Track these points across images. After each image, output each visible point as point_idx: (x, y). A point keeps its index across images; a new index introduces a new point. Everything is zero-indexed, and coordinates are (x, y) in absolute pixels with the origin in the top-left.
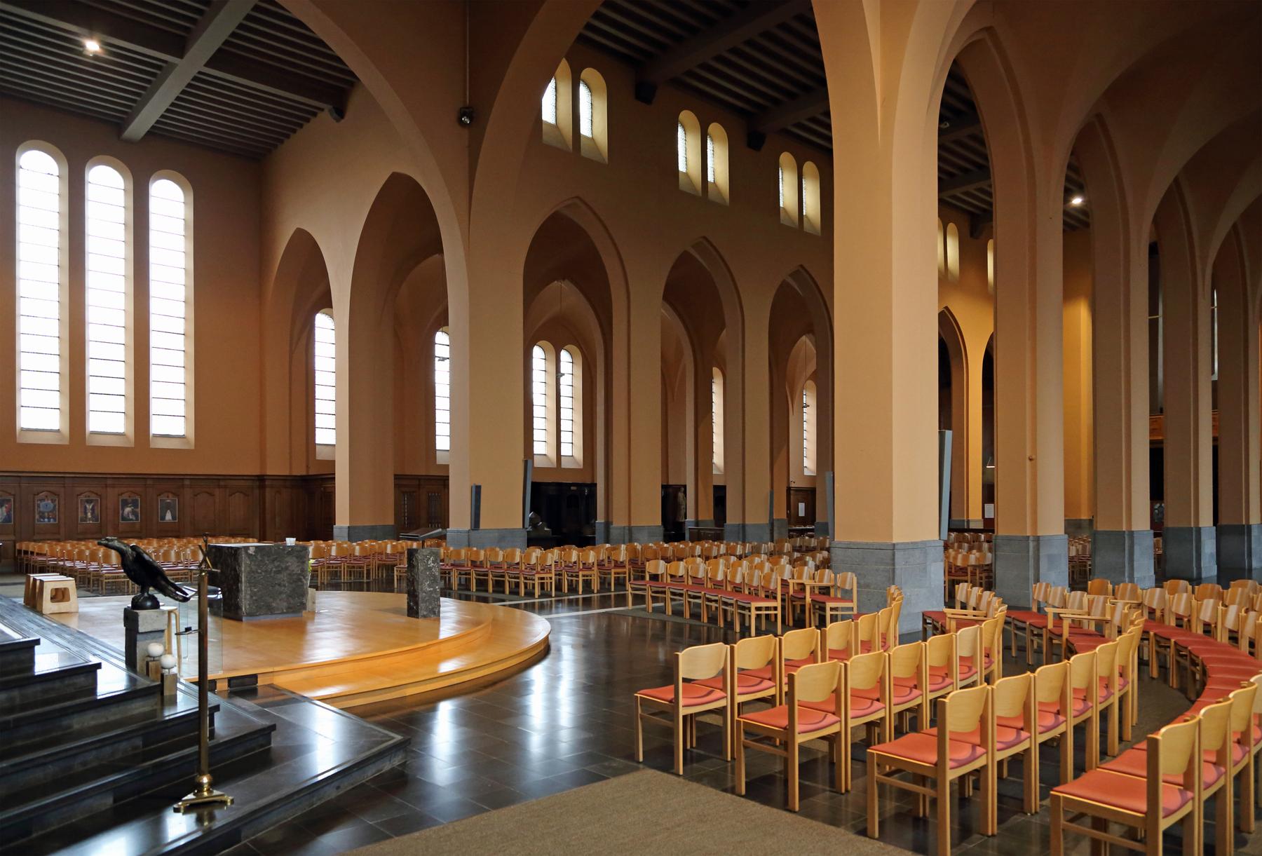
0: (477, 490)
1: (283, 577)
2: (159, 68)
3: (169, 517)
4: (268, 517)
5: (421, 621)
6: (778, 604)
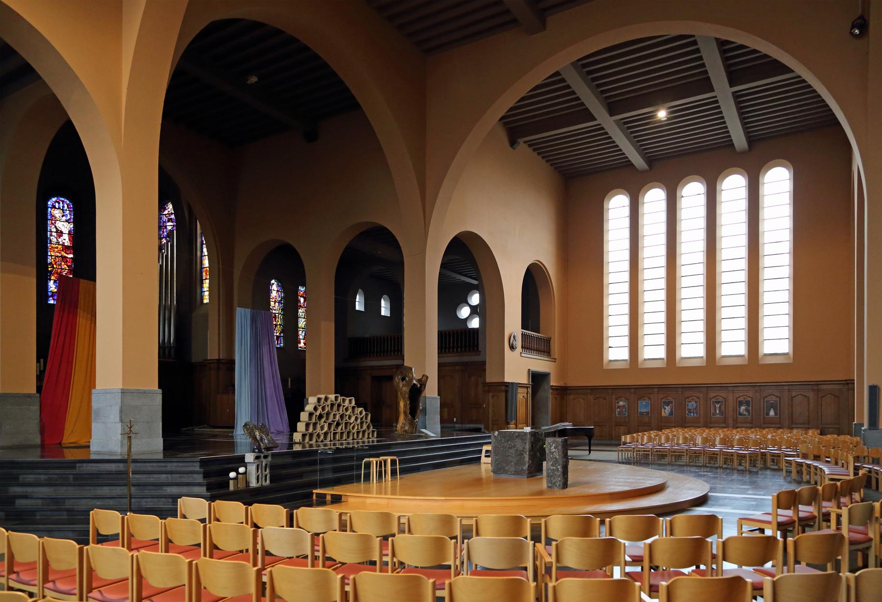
3: (772, 413)
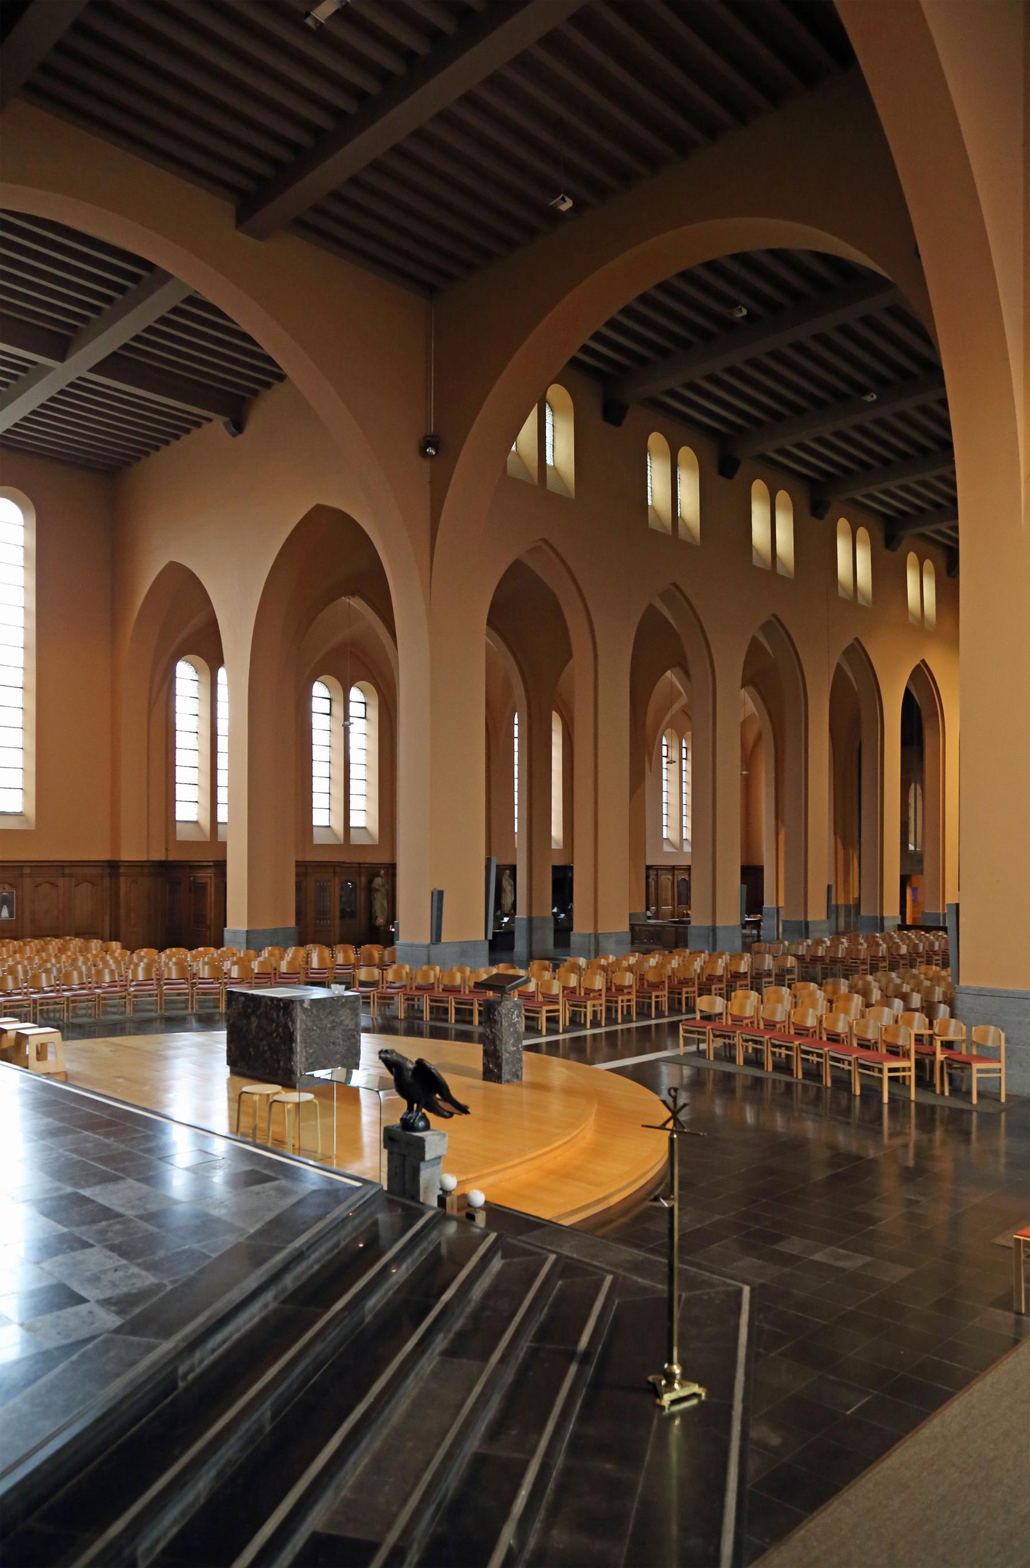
0: (438, 898)
1: (338, 1034)
2: (24, 369)
4: (122, 912)
5: (503, 1087)
6: (911, 1064)
